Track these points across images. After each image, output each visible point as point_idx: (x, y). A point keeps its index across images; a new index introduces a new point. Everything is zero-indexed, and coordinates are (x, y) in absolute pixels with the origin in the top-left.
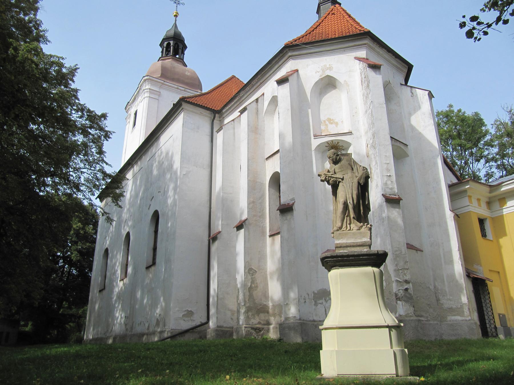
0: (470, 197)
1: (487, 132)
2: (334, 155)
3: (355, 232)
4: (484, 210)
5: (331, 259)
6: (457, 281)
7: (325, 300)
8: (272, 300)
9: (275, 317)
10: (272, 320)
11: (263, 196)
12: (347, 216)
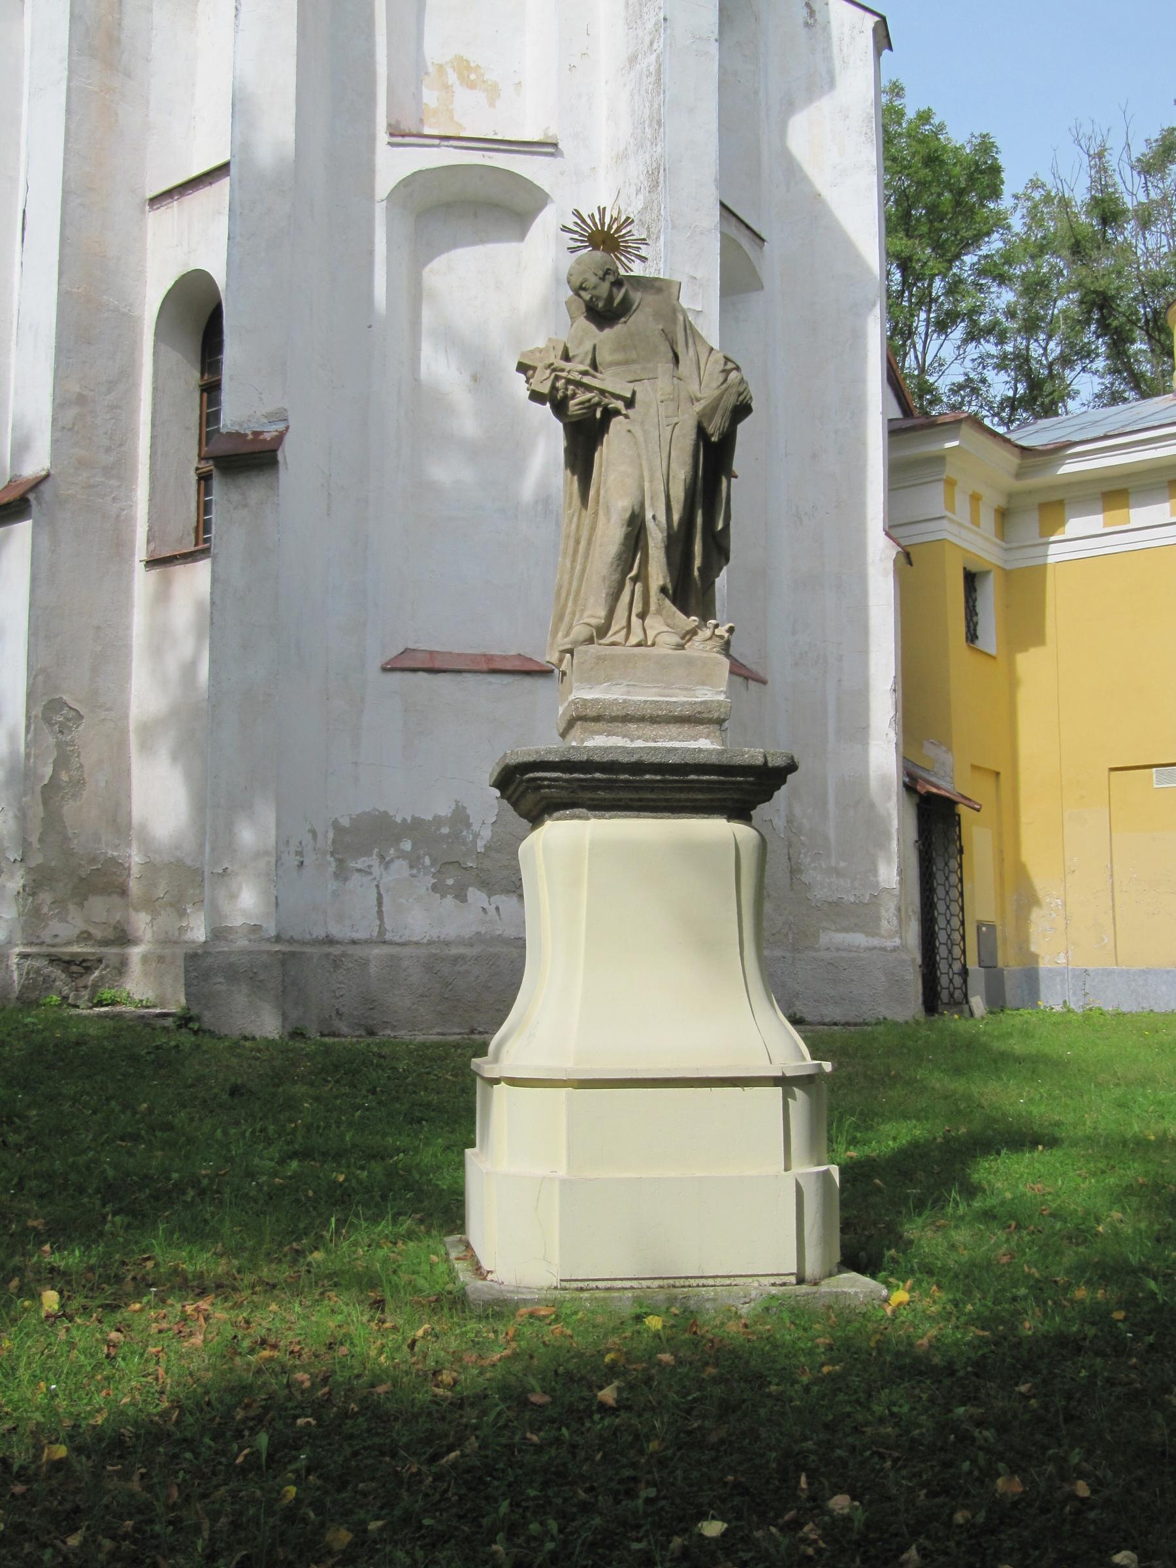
0: (951, 483)
1: (999, 222)
2: (603, 279)
3: (666, 656)
4: (986, 539)
5: (560, 775)
6: (872, 806)
7: (382, 857)
8: (146, 844)
9: (155, 914)
10: (142, 923)
11: (126, 375)
12: (635, 580)
